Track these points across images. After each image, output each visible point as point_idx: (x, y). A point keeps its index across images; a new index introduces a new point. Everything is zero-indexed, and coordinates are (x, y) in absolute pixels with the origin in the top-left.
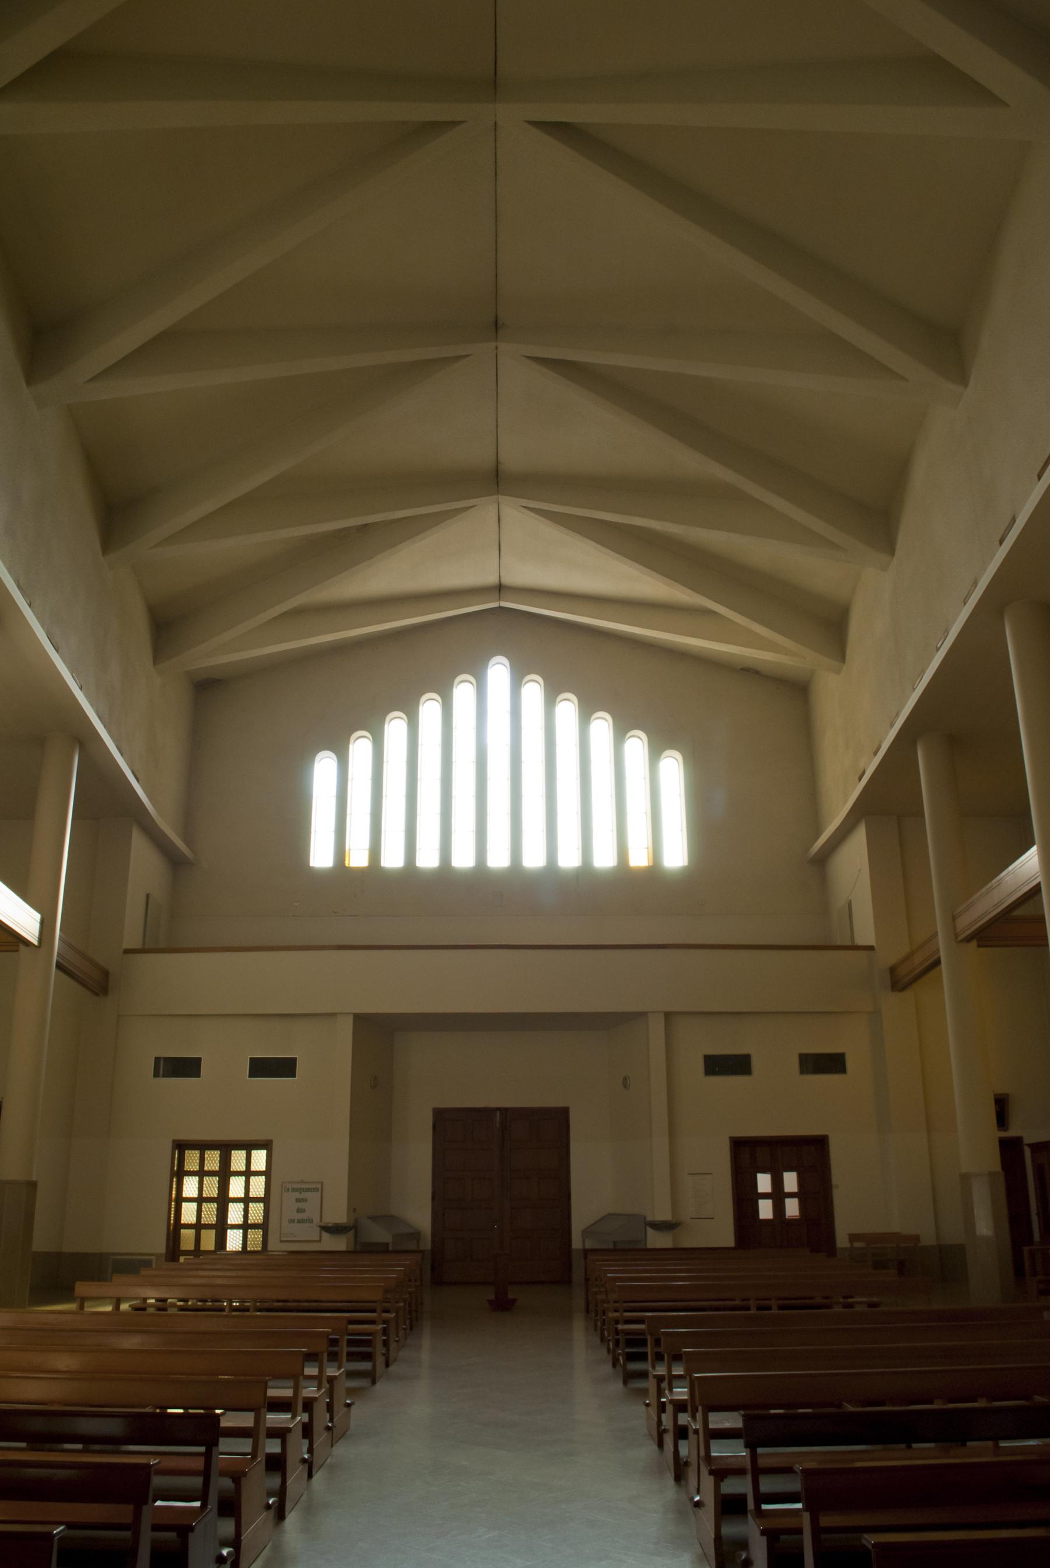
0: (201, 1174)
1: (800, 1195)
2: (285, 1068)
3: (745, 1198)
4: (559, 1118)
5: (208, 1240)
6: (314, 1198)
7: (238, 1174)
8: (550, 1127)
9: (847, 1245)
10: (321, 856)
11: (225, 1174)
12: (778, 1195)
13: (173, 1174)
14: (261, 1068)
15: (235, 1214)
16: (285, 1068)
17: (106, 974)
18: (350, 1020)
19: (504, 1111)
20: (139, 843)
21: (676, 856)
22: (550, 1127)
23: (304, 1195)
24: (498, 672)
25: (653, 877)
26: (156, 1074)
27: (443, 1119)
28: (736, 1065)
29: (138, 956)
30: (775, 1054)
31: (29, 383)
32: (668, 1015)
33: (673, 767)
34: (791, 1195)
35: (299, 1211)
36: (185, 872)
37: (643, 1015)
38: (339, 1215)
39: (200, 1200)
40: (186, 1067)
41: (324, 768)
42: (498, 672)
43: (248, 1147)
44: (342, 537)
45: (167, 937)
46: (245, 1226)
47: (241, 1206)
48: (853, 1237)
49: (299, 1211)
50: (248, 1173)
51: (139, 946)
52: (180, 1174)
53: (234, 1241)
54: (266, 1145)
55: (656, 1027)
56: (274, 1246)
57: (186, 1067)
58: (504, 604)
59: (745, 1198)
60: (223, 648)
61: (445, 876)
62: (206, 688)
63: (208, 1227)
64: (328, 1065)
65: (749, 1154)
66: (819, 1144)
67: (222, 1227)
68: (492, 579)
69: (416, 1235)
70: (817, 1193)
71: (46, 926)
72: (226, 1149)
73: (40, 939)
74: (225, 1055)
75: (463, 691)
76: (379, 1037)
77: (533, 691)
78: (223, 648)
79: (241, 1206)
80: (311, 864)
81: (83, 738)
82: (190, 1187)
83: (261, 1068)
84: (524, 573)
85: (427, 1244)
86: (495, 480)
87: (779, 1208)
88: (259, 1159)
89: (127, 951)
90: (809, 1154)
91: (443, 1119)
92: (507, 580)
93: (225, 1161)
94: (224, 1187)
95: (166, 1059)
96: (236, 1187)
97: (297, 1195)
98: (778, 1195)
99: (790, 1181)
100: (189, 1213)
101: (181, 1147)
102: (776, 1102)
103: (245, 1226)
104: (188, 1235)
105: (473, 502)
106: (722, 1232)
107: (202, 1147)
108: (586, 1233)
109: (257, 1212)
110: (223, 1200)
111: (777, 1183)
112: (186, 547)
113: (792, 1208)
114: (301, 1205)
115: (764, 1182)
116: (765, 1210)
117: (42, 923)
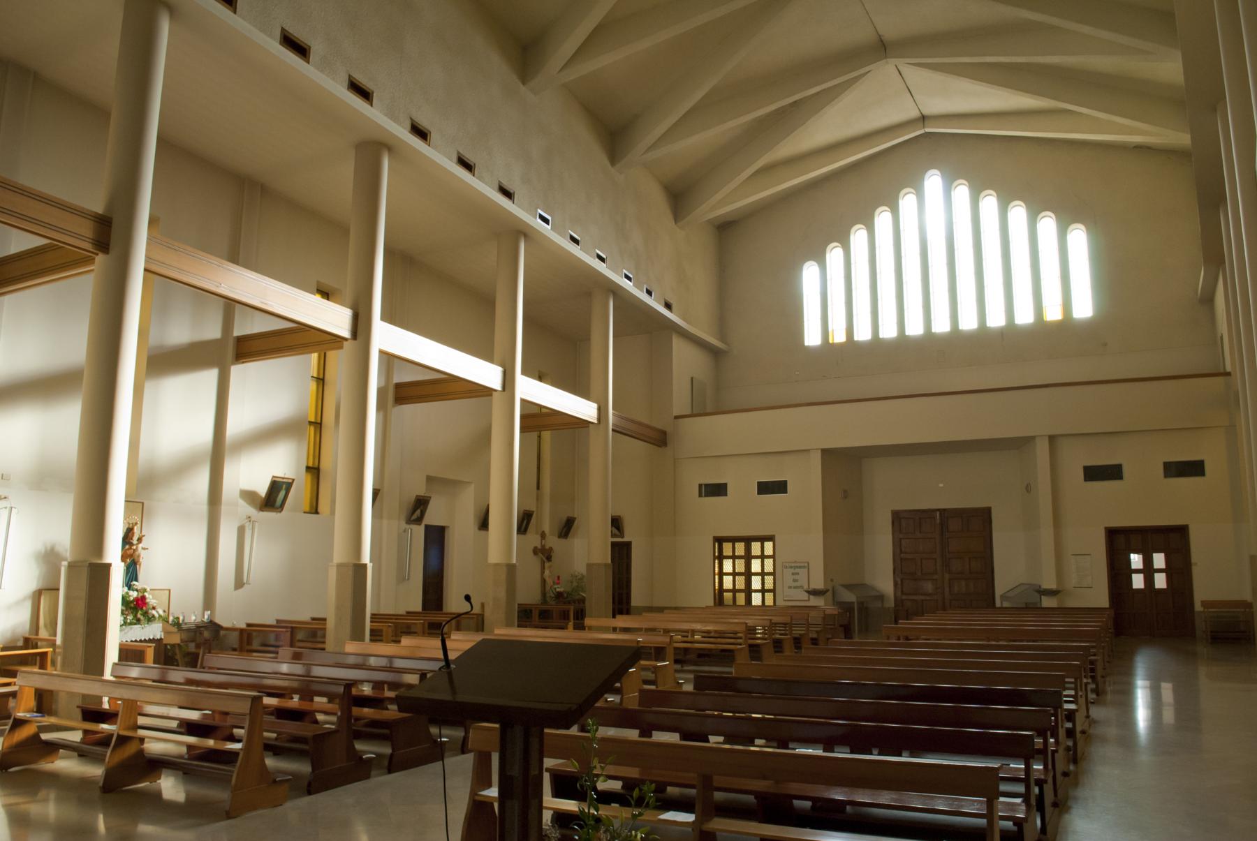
0: (734, 557)
1: (1168, 570)
2: (779, 487)
3: (1118, 573)
4: (983, 517)
5: (741, 599)
6: (803, 572)
7: (757, 557)
8: (978, 522)
9: (1201, 609)
10: (812, 338)
11: (748, 558)
12: (1148, 571)
13: (715, 558)
14: (766, 488)
15: (756, 583)
16: (779, 487)
17: (664, 433)
18: (819, 454)
19: (942, 511)
20: (678, 344)
21: (1084, 309)
22: (978, 522)
23: (797, 570)
24: (933, 181)
25: (1067, 327)
26: (700, 495)
27: (897, 517)
28: (1112, 473)
29: (686, 420)
30: (1145, 466)
31: (524, 84)
32: (1052, 439)
33: (1079, 238)
34: (1160, 571)
35: (795, 581)
36: (747, 353)
37: (1033, 438)
38: (818, 584)
39: (734, 574)
40: (717, 490)
41: (810, 272)
42: (933, 181)
43: (762, 540)
44: (781, 113)
45: (712, 401)
46: (763, 591)
47: (731, 578)
48: (1204, 603)
49: (795, 581)
50: (763, 557)
51: (688, 412)
52: (721, 558)
53: (756, 599)
54: (771, 538)
55: (1042, 448)
56: (780, 603)
57: (717, 490)
58: (928, 130)
59: (1118, 573)
60: (724, 200)
61: (903, 344)
62: (725, 229)
63: (740, 591)
64: (807, 482)
65: (1119, 541)
66: (1182, 531)
67: (748, 591)
68: (914, 113)
69: (881, 597)
70: (1180, 570)
71: (602, 411)
72: (748, 541)
73: (599, 419)
74: (742, 481)
75: (907, 202)
76: (845, 466)
77: (962, 192)
78: (724, 200)
79: (759, 578)
80: (806, 344)
81: (615, 291)
82: (728, 566)
83: (766, 488)
84: (935, 106)
85: (890, 603)
86: (882, 48)
87: (1149, 580)
88: (769, 547)
89: (676, 417)
90: (1172, 539)
91: (897, 517)
92: (926, 112)
93: (748, 549)
94: (748, 566)
95: (706, 485)
96: (756, 566)
97: (792, 570)
98: (1148, 571)
99: (1159, 560)
100: (728, 582)
101: (720, 540)
102: (1144, 499)
103: (763, 591)
104: (728, 596)
105: (867, 69)
106: (1100, 597)
107: (734, 540)
108: (1003, 597)
109: (769, 582)
110: (748, 574)
111: (1148, 561)
112: (673, 143)
113: (1160, 581)
114: (796, 577)
115: (1136, 560)
116: (1138, 582)
117: (599, 409)
